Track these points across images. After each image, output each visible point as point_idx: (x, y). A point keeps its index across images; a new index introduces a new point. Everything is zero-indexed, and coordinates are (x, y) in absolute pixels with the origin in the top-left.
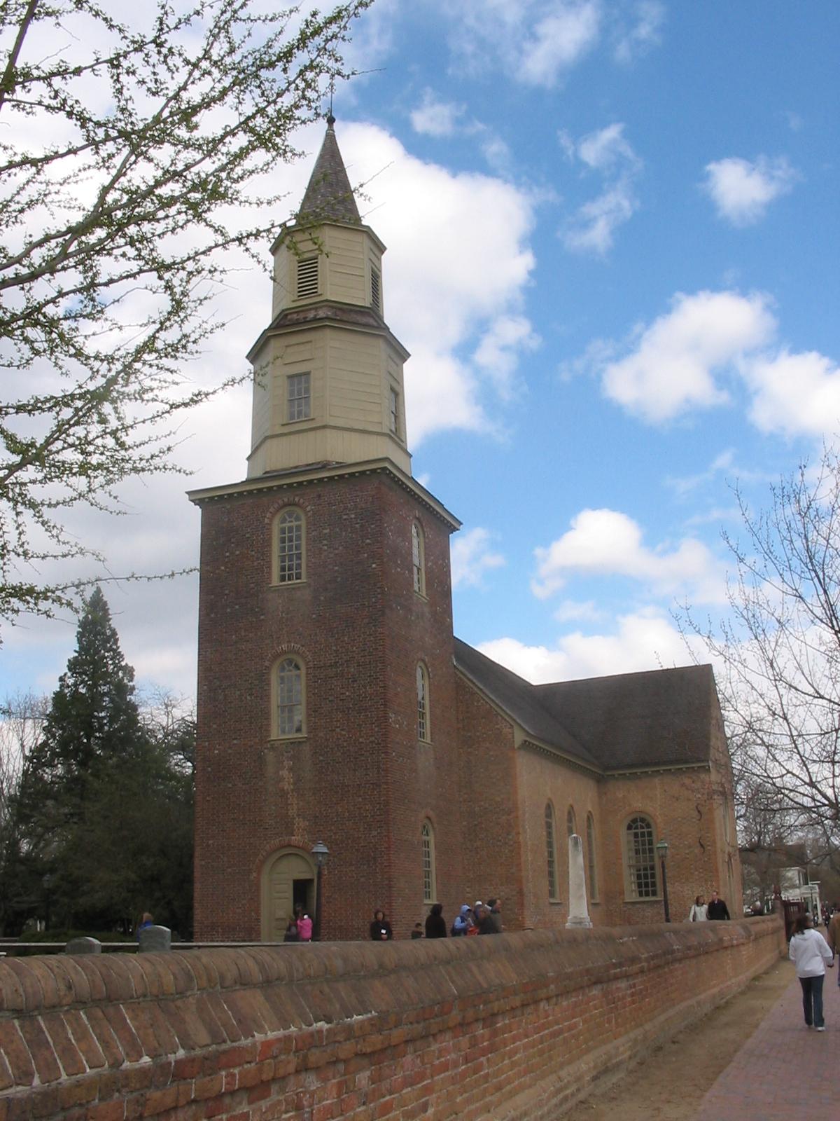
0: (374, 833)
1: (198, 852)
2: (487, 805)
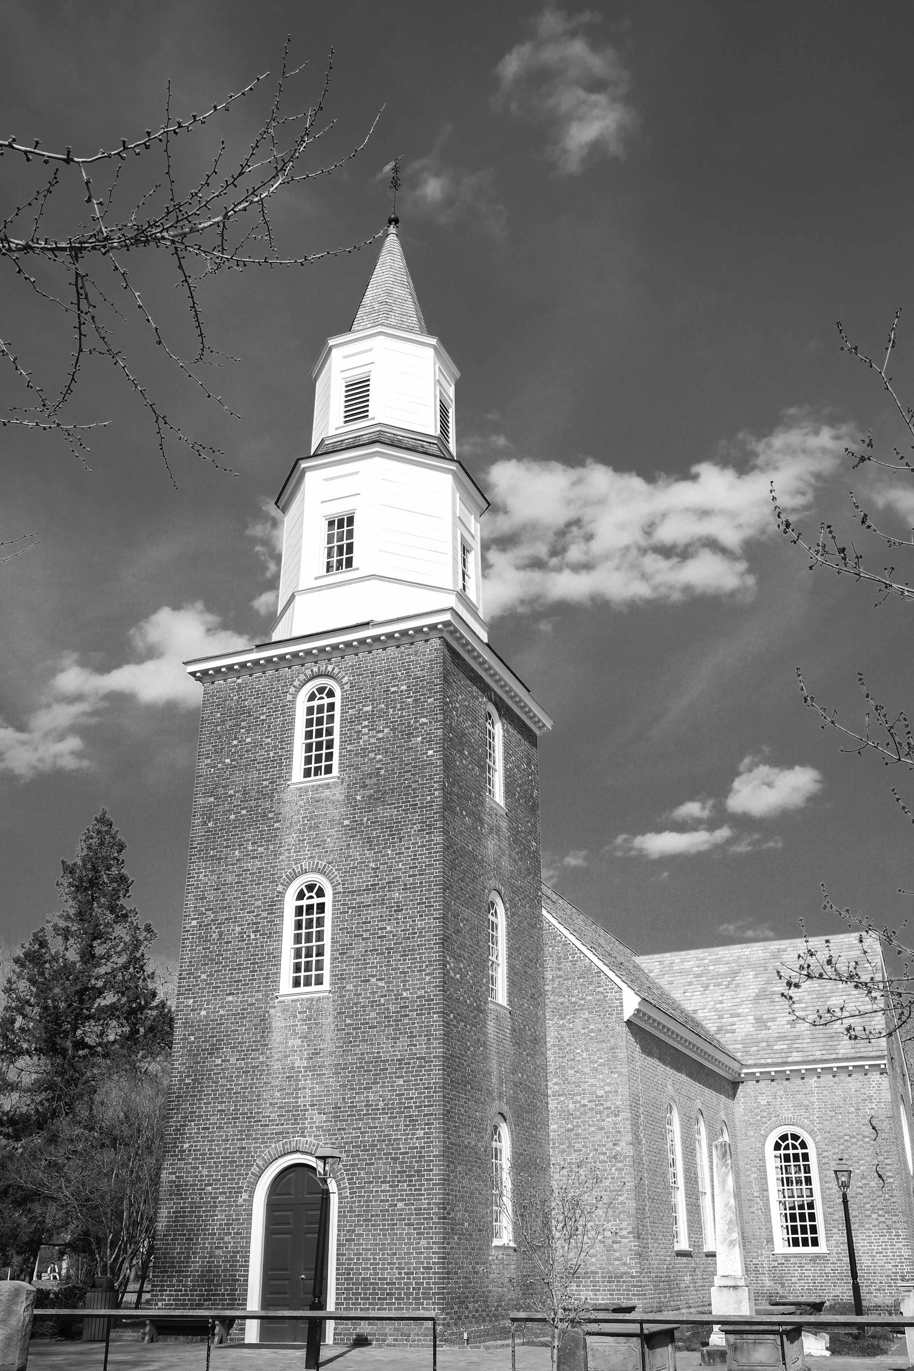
0: (420, 1133)
2: (586, 1102)
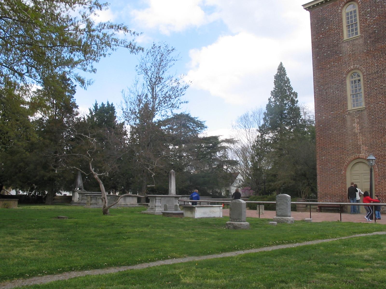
1: (318, 162)
